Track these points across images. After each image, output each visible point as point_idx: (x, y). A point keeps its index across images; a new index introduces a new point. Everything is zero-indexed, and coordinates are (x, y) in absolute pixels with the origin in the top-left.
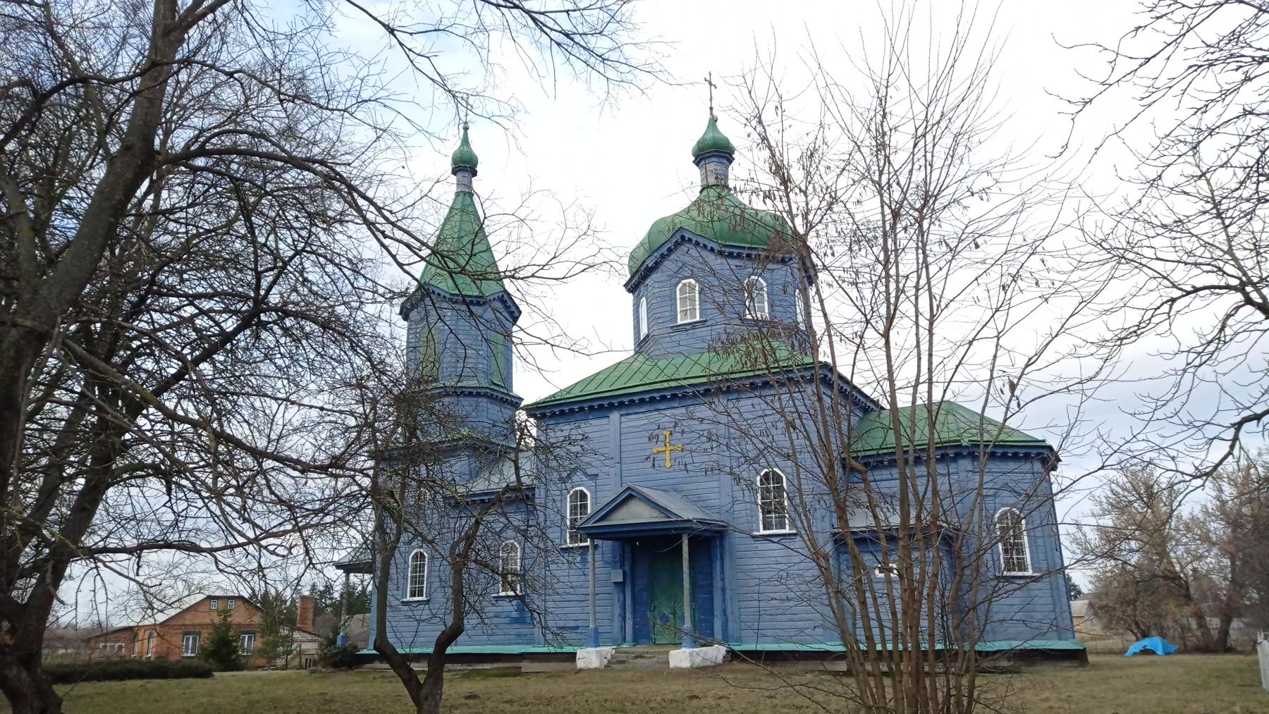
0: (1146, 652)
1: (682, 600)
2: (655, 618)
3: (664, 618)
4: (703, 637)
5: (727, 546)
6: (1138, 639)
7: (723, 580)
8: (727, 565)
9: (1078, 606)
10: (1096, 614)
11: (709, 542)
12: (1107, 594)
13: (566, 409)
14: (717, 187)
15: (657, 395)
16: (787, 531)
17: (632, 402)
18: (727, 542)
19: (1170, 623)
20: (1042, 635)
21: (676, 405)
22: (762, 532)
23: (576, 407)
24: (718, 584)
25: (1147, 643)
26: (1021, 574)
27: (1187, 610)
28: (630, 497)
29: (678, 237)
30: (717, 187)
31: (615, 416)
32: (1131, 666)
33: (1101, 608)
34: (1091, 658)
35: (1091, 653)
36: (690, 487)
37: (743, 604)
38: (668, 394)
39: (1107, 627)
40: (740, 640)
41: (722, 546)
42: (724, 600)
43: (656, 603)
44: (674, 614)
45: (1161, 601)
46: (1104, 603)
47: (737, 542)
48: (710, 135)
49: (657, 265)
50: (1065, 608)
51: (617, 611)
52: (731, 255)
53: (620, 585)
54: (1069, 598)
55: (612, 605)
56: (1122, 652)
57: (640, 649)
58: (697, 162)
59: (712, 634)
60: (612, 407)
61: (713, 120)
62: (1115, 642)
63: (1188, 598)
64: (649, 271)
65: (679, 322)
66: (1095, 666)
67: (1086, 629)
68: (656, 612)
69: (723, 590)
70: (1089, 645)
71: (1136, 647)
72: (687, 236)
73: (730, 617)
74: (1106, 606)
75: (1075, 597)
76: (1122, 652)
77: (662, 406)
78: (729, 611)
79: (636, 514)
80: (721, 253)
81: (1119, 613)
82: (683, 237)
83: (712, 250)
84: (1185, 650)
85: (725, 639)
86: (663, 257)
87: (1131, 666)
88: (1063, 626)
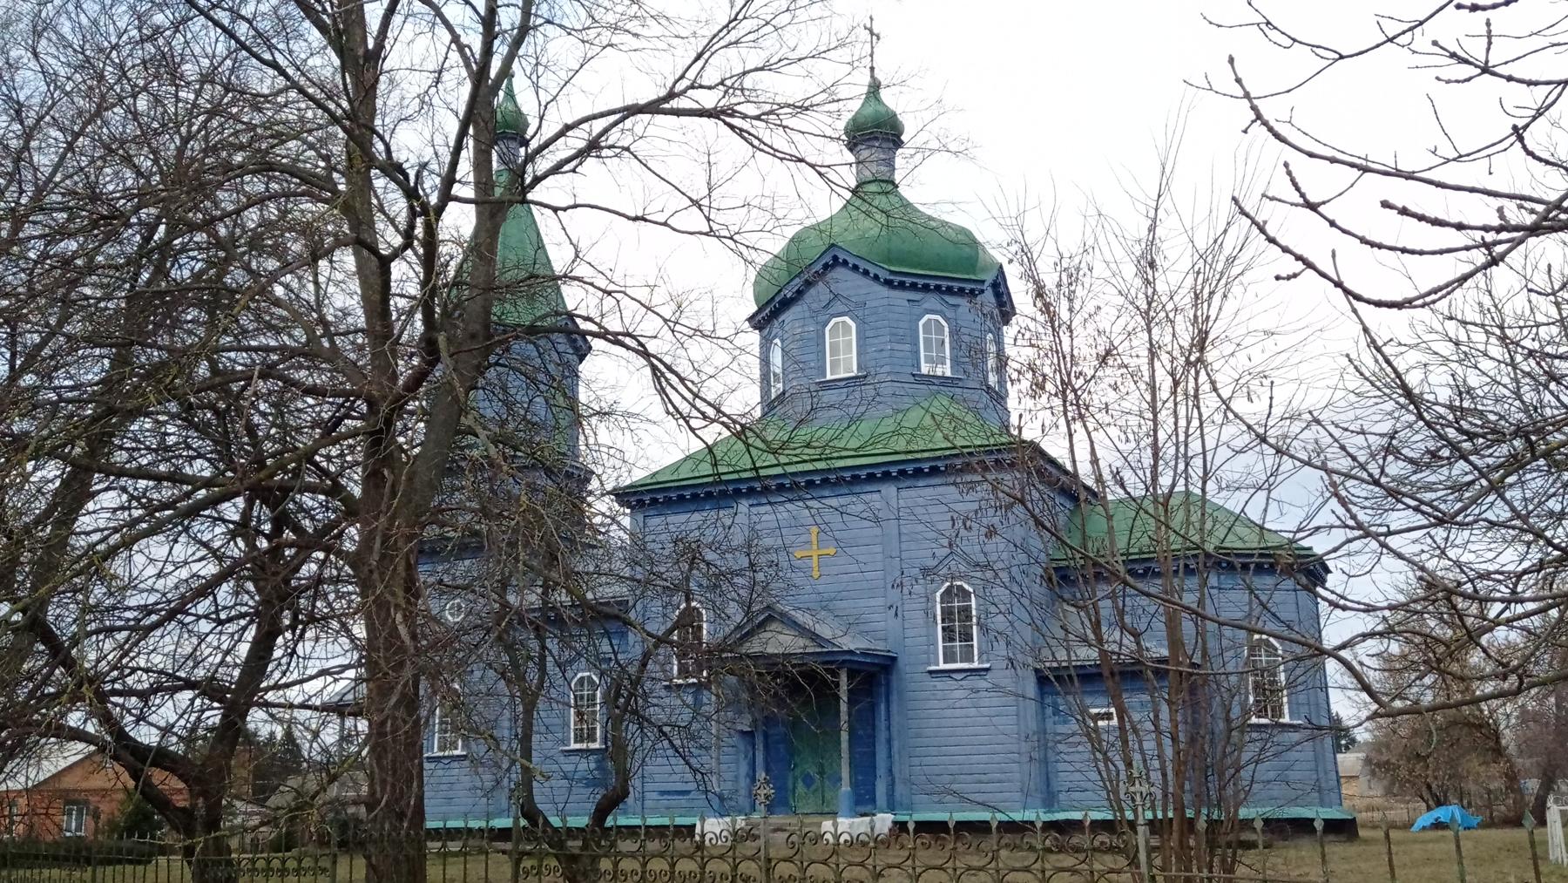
0: (1438, 825)
1: (840, 757)
2: (795, 779)
3: (808, 781)
4: (864, 802)
5: (894, 684)
6: (1429, 809)
7: (889, 728)
8: (894, 708)
9: (1349, 761)
10: (1373, 773)
11: (874, 676)
12: (1388, 747)
13: (673, 495)
14: (875, 189)
15: (847, 475)
16: (976, 665)
17: (856, 478)
18: (894, 677)
19: (1472, 787)
20: (1294, 802)
21: (826, 493)
22: (942, 666)
23: (687, 493)
24: (882, 736)
25: (1441, 813)
26: (965, 666)
27: (1495, 769)
28: (770, 619)
29: (828, 259)
30: (875, 189)
31: (743, 506)
32: (1415, 841)
33: (1378, 765)
34: (1362, 833)
35: (1363, 826)
36: (844, 604)
37: (916, 761)
38: (817, 479)
39: (1388, 792)
40: (910, 808)
41: (888, 685)
42: (890, 756)
43: (797, 760)
44: (821, 773)
45: (1463, 756)
46: (1385, 758)
47: (910, 673)
48: (870, 110)
49: (800, 293)
50: (1330, 766)
51: (744, 768)
52: (902, 286)
53: (748, 736)
54: (1337, 749)
55: (737, 762)
56: (1407, 826)
57: (776, 820)
58: (851, 150)
59: (873, 801)
60: (738, 494)
61: (875, 88)
62: (1398, 813)
63: (1498, 751)
64: (786, 304)
65: (829, 377)
66: (1366, 841)
67: (1359, 794)
68: (798, 772)
69: (889, 741)
70: (1362, 817)
71: (1426, 819)
72: (841, 257)
73: (897, 775)
74: (1387, 762)
75: (1347, 748)
76: (1407, 826)
77: (857, 489)
78: (896, 770)
79: (778, 642)
80: (888, 283)
81: (1403, 773)
82: (835, 258)
83: (876, 277)
84: (1490, 824)
85: (891, 808)
86: (809, 284)
87: (1415, 841)
88: (1328, 785)
